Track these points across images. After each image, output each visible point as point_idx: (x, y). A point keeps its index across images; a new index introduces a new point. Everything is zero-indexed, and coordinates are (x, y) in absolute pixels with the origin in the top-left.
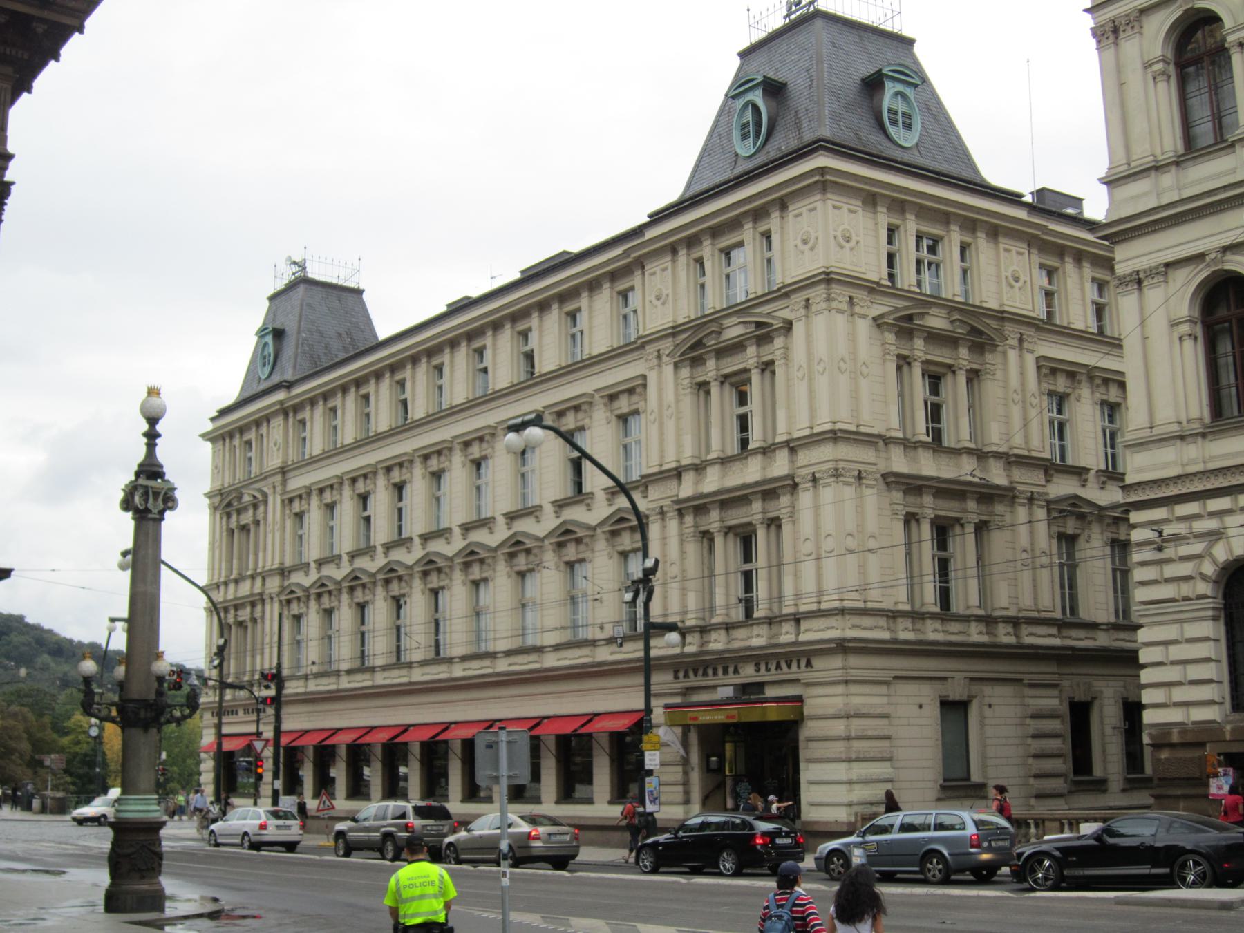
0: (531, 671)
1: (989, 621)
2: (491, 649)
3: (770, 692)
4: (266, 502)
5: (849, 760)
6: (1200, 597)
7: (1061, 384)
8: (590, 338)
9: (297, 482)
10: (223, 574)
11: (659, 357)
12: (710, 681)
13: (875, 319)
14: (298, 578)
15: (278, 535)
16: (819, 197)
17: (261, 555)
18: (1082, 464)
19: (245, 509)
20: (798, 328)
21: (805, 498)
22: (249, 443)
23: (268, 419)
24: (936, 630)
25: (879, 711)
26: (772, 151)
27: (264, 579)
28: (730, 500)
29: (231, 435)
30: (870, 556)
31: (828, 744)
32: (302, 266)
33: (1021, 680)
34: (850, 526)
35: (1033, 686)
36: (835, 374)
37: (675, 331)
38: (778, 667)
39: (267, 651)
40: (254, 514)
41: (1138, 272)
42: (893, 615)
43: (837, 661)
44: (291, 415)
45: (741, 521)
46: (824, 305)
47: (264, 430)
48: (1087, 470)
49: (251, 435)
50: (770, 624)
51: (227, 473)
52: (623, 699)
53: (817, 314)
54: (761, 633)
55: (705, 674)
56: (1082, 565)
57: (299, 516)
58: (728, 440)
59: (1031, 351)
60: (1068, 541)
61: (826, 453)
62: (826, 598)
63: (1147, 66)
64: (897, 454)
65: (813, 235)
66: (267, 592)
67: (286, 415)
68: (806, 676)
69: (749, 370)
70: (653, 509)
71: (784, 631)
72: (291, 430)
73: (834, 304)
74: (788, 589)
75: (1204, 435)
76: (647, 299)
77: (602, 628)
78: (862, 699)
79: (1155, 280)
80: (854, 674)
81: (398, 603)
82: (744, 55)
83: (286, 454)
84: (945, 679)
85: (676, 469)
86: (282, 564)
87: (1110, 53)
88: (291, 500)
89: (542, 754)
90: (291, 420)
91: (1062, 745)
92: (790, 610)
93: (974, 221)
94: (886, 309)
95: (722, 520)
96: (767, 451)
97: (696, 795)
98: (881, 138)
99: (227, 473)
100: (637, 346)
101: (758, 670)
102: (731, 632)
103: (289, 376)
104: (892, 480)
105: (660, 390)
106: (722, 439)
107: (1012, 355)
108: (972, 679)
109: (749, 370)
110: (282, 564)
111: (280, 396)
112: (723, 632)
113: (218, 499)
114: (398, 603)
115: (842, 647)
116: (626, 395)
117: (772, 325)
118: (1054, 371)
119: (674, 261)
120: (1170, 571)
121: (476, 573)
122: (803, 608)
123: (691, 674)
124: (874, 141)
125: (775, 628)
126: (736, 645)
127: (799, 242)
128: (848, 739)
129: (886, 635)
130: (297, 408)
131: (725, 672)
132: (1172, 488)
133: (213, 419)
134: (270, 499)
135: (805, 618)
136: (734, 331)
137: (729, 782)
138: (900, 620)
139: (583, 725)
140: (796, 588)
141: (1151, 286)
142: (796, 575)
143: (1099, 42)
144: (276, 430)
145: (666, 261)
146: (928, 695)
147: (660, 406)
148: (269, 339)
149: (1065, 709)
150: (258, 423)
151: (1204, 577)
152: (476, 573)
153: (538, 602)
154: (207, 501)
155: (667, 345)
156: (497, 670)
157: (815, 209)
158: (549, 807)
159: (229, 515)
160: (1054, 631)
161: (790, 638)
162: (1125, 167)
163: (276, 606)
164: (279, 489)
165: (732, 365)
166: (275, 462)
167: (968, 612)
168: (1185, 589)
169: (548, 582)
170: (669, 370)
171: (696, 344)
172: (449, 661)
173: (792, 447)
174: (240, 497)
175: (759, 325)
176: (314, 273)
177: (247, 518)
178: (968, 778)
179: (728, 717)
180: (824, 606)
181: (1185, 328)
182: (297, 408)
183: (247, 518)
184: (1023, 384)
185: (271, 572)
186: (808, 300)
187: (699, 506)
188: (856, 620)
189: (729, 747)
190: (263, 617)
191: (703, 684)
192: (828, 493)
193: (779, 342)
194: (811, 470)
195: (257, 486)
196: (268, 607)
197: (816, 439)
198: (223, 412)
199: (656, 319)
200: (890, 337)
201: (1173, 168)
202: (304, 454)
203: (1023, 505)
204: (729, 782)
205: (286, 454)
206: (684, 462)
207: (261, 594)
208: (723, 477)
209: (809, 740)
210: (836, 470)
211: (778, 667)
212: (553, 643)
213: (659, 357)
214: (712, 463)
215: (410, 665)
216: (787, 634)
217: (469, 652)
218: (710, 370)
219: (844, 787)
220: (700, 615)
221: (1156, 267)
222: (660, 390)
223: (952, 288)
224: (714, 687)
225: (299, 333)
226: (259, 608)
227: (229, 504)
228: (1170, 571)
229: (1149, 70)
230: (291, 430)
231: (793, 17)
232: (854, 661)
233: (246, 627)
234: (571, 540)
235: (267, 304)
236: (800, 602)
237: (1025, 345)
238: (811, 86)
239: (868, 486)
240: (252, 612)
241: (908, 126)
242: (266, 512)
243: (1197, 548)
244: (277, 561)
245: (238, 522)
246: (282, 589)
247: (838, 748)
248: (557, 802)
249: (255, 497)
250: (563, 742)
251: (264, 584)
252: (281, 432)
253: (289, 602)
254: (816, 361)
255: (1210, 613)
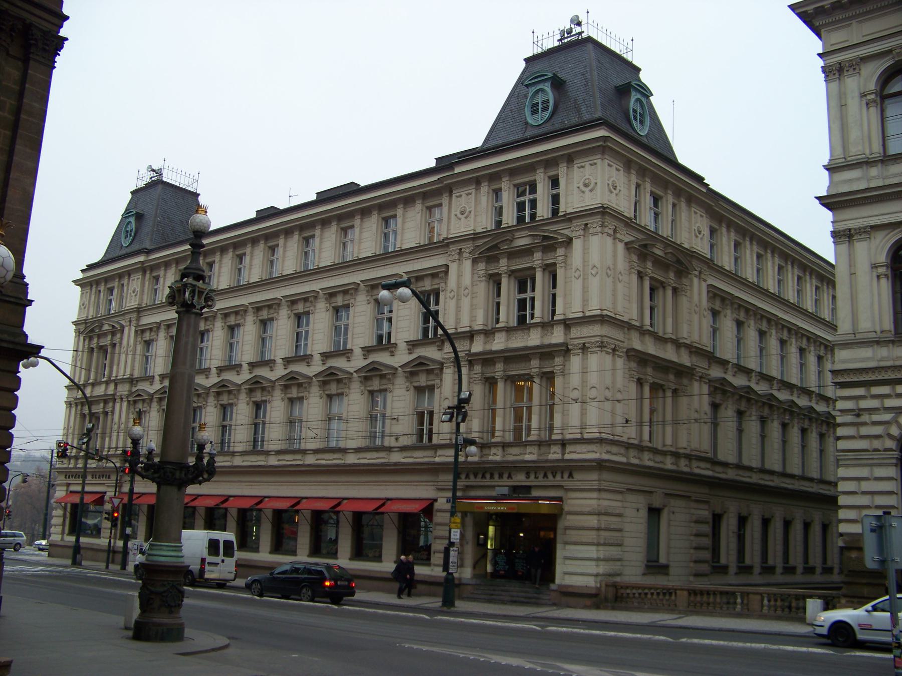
0: (373, 465)
1: (676, 455)
2: (342, 445)
3: (535, 493)
4: (122, 331)
5: (598, 544)
6: (886, 450)
7: (717, 305)
8: (402, 237)
9: (147, 320)
10: (82, 379)
11: (460, 252)
12: (488, 482)
13: (626, 244)
14: (144, 386)
15: (130, 357)
16: (599, 156)
17: (115, 368)
18: (725, 358)
19: (105, 335)
20: (577, 244)
21: (575, 362)
22: (111, 290)
23: (129, 274)
24: (649, 459)
25: (617, 512)
26: (557, 124)
27: (116, 385)
28: (511, 357)
29: (98, 283)
30: (618, 405)
31: (581, 532)
32: (159, 173)
33: (689, 497)
34: (608, 382)
35: (697, 501)
36: (594, 277)
37: (475, 237)
38: (545, 476)
39: (115, 435)
40: (112, 339)
41: (850, 230)
42: (628, 446)
43: (594, 476)
44: (148, 272)
45: (528, 370)
46: (599, 229)
47: (125, 281)
48: (728, 362)
49: (116, 284)
50: (539, 445)
51: (91, 309)
52: (409, 491)
53: (593, 234)
54: (533, 451)
55: (483, 477)
56: (722, 424)
57: (148, 344)
58: (511, 316)
59: (705, 281)
60: (715, 406)
61: (596, 330)
62: (588, 430)
63: (863, 95)
64: (635, 335)
65: (593, 182)
66: (118, 394)
67: (144, 272)
68: (568, 483)
69: (535, 268)
70: (448, 359)
71: (552, 451)
72: (147, 283)
73: (606, 230)
74: (558, 421)
75: (893, 342)
76: (453, 213)
77: (397, 439)
78: (610, 502)
79: (863, 236)
80: (604, 485)
81: (225, 409)
82: (527, 60)
83: (142, 299)
84: (651, 492)
85: (469, 332)
86: (132, 375)
87: (834, 85)
88: (143, 331)
89: (262, 520)
90: (148, 276)
91: (707, 542)
92: (559, 437)
93: (681, 189)
94: (633, 239)
95: (504, 371)
96: (546, 326)
97: (67, 531)
98: (628, 127)
99: (91, 309)
100: (445, 245)
101: (528, 476)
102: (506, 449)
103: (148, 245)
104: (633, 355)
105: (460, 276)
106: (508, 315)
107: (696, 280)
108: (666, 494)
109: (535, 268)
110: (132, 375)
111: (141, 258)
112: (500, 449)
113: (82, 327)
114: (225, 409)
115: (600, 466)
116: (430, 278)
117: (557, 239)
118: (715, 296)
119: (91, 289)
120: (864, 431)
121: (294, 393)
122: (568, 437)
123: (472, 477)
124: (624, 127)
125: (543, 449)
126: (511, 458)
127: (581, 185)
128: (598, 529)
129: (624, 460)
130: (153, 268)
131: (501, 476)
132: (870, 375)
133: (83, 271)
134: (126, 330)
135: (569, 444)
136: (522, 241)
137: (490, 554)
138: (631, 450)
139: (192, 500)
140: (563, 423)
141: (859, 240)
142: (564, 413)
143: (826, 76)
144: (135, 283)
145: (472, 189)
146: (641, 502)
147: (459, 287)
148: (132, 220)
149: (710, 518)
150: (120, 276)
151: (890, 436)
152: (294, 393)
153: (344, 416)
154: (74, 327)
155: (468, 247)
156: (307, 462)
157: (595, 164)
158: (264, 555)
159: (91, 339)
160: (708, 466)
161: (558, 456)
162: (843, 160)
163: (125, 404)
164: (134, 323)
165: (520, 264)
166: (132, 303)
167: (665, 449)
168: (877, 444)
169: (355, 402)
170: (468, 264)
171: (490, 248)
172: (267, 453)
173: (567, 324)
174: (101, 326)
175: (545, 238)
176: (167, 177)
177: (106, 341)
178: (657, 561)
179: (509, 508)
180: (586, 436)
181: (883, 270)
182: (153, 268)
183: (106, 341)
184: (700, 301)
185: (123, 381)
186: (586, 225)
187: (487, 359)
188: (609, 448)
189: (491, 529)
190: (113, 412)
191: (482, 484)
192: (594, 360)
193: (560, 251)
194: (583, 341)
195: (116, 319)
196: (118, 405)
197: (586, 320)
198: (91, 267)
199: (460, 227)
200: (635, 258)
201: (880, 165)
202: (155, 300)
203: (696, 380)
204: (490, 554)
205: (142, 299)
206: (476, 328)
207: (114, 395)
208: (485, 343)
209: (567, 528)
210: (602, 342)
211: (545, 476)
212: (354, 446)
213: (460, 252)
214: (500, 330)
215: (233, 454)
216: (554, 454)
217: (283, 447)
218: (503, 265)
219: (594, 563)
220: (481, 435)
221: (865, 228)
222: (460, 276)
223: (665, 231)
224: (494, 487)
225: (156, 217)
226: (111, 404)
227: (92, 331)
228: (864, 431)
229: (864, 99)
230: (147, 283)
231: (566, 41)
232: (606, 475)
233: (99, 418)
234: (376, 376)
235: (130, 196)
236: (565, 432)
237: (702, 276)
238: (586, 85)
239: (592, 353)
240: (104, 408)
241: (642, 122)
242: (121, 339)
243: (887, 417)
244: (128, 372)
245: (98, 343)
246: (131, 393)
247: (591, 536)
248: (271, 553)
249: (113, 326)
250: (358, 517)
251: (116, 388)
252: (139, 283)
253: (135, 402)
254: (590, 267)
255: (894, 461)
